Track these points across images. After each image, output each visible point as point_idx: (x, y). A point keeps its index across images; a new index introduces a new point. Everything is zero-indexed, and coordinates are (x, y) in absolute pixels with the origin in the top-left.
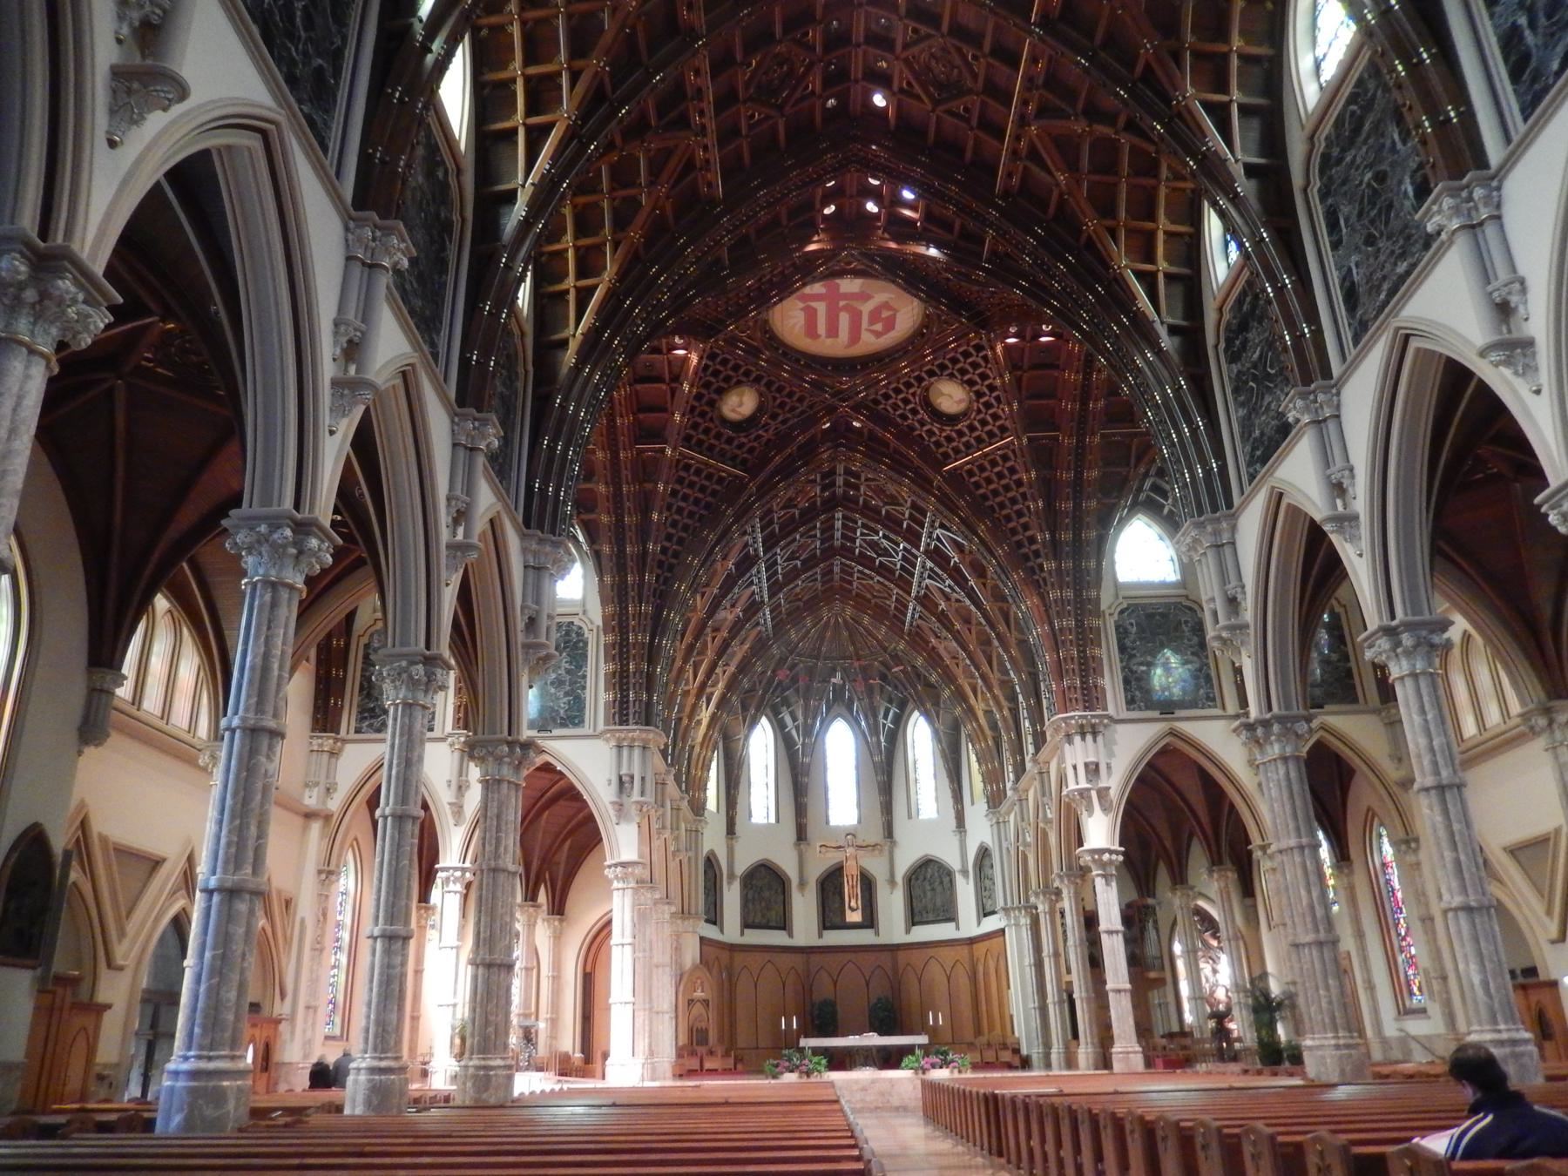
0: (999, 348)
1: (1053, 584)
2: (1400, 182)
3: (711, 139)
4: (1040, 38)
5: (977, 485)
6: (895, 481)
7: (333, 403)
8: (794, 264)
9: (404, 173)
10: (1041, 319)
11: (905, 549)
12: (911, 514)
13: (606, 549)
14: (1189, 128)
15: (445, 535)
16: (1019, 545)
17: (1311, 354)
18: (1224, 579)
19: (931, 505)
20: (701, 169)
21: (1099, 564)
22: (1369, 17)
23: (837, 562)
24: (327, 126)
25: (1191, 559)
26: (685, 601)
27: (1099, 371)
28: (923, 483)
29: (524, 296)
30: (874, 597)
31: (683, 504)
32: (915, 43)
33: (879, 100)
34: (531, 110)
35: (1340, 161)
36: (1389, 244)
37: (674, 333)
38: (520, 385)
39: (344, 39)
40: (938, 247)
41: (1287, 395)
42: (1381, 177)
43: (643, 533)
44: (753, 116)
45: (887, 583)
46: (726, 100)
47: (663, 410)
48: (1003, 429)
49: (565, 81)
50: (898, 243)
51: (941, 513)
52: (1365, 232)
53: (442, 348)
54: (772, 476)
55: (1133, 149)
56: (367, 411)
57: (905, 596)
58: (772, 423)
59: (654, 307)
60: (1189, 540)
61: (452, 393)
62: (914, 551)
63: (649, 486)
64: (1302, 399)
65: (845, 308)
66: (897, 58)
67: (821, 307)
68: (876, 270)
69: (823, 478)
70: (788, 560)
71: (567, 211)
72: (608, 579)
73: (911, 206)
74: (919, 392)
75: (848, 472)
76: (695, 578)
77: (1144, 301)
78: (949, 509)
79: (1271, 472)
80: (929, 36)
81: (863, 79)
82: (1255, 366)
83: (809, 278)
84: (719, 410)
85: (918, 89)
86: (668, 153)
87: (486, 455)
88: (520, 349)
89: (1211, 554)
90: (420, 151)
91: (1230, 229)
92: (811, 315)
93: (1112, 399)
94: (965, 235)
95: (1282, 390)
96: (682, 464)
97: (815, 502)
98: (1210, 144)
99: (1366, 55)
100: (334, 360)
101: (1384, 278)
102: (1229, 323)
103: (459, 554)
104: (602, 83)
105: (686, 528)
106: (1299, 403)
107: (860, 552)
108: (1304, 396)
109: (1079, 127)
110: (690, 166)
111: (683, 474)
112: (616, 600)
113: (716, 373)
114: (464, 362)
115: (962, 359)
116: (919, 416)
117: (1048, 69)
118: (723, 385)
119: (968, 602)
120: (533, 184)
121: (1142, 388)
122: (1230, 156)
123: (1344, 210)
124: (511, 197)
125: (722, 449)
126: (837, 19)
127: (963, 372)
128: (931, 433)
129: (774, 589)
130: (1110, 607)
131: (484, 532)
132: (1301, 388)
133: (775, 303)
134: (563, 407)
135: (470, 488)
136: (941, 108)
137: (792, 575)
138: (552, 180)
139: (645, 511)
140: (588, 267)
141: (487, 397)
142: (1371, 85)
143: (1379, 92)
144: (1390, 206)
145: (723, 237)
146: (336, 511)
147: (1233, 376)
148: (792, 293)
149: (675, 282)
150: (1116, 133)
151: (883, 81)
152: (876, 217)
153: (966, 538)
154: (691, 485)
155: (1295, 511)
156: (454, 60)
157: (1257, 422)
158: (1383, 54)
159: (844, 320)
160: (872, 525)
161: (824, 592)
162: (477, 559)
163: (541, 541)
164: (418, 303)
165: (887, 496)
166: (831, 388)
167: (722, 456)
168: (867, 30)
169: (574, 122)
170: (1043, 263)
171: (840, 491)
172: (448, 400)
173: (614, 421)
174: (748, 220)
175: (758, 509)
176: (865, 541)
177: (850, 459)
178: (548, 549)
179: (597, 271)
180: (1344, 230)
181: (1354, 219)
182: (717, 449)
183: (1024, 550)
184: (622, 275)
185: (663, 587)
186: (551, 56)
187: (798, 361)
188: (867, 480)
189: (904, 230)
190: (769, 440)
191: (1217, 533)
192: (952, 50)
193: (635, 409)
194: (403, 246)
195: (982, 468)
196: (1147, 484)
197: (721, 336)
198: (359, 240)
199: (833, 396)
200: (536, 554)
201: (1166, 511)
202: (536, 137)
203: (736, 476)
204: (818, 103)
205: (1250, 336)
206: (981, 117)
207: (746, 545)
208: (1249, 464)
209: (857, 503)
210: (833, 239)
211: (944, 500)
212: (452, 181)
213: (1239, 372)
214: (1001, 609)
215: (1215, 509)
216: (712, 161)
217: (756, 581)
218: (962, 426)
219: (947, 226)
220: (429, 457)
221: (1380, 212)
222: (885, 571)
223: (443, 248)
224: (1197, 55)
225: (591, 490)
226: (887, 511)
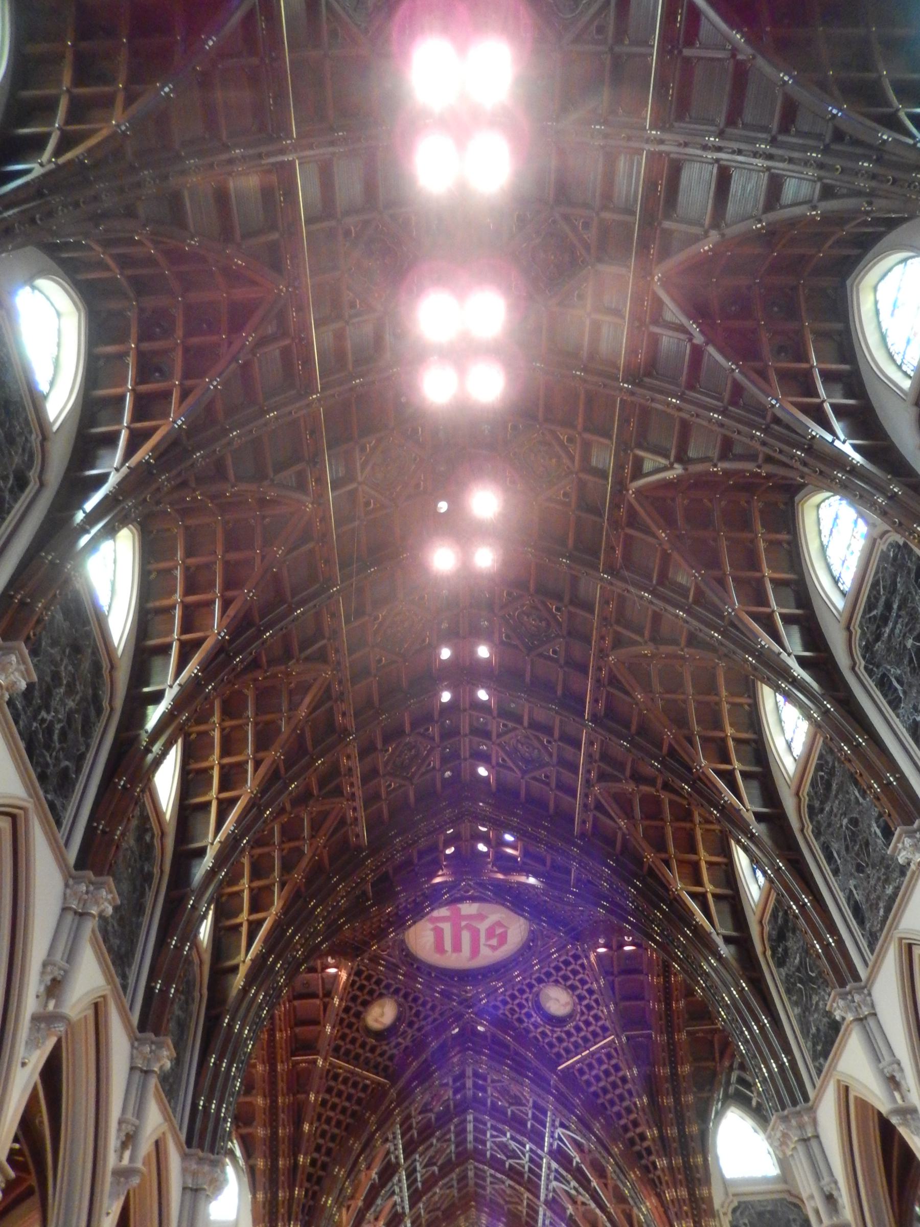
0: (592, 957)
1: (667, 1184)
2: (869, 826)
3: (359, 803)
4: (593, 729)
5: (588, 1083)
6: (517, 1081)
7: (29, 1037)
8: (424, 894)
9: (119, 839)
10: (622, 932)
11: (531, 1150)
12: (533, 1114)
13: (260, 1163)
14: (709, 788)
15: (111, 1161)
16: (632, 1142)
17: (839, 958)
18: (818, 1177)
19: (550, 1103)
20: (351, 825)
21: (705, 1160)
22: (815, 715)
23: (471, 1165)
24: (64, 808)
25: (784, 1154)
26: (332, 1216)
27: (675, 975)
28: (540, 1081)
29: (205, 931)
30: (507, 1202)
31: (331, 1114)
32: (506, 733)
33: (482, 771)
34: (223, 788)
35: (822, 810)
36: (874, 871)
37: (327, 955)
38: (195, 1007)
39: (88, 746)
40: (535, 876)
41: (829, 995)
42: (854, 822)
43: (295, 1147)
44: (390, 785)
45: (517, 1187)
46: (370, 775)
47: (316, 1022)
48: (604, 1029)
49: (250, 767)
50: (505, 874)
51: (560, 1112)
52: (854, 862)
53: (131, 980)
54: (409, 1082)
55: (671, 802)
56: (59, 1041)
57: (535, 1200)
58: (410, 1031)
59: (311, 934)
60: (779, 1135)
61: (135, 1018)
62: (539, 1152)
63: (301, 1097)
64: (843, 999)
65: (468, 927)
66: (493, 743)
67: (447, 927)
68: (489, 896)
69: (455, 1081)
70: (426, 1166)
71: (246, 861)
72: (260, 1196)
73: (513, 846)
74: (531, 996)
75: (476, 1074)
76: (341, 1190)
77: (700, 917)
78: (565, 1106)
79: (833, 1066)
80: (514, 729)
81: (470, 709)
82: (798, 970)
83: (437, 904)
84: (364, 1020)
85: (510, 763)
86: (324, 815)
87: (159, 1077)
88: (198, 979)
89: (801, 1148)
90: (134, 823)
91: (753, 860)
92: (439, 933)
93: (690, 999)
94: (555, 867)
95: (824, 991)
96: (331, 1074)
97: (448, 1106)
98: (726, 799)
99: (820, 741)
100: (38, 997)
101: (879, 898)
102: (770, 935)
103: (122, 1179)
104: (277, 768)
105: (333, 1138)
106: (841, 1003)
107: (492, 1155)
108: (843, 996)
109: (630, 787)
110: (342, 822)
111: (332, 1083)
112: (267, 1219)
113: (362, 988)
114: (149, 990)
115: (564, 967)
116: (533, 1020)
117: (601, 749)
118: (367, 997)
119: (593, 1205)
120: (220, 842)
121: (711, 988)
122: (742, 807)
123: (835, 846)
124: (201, 852)
125: (367, 1058)
126: (449, 719)
127: (566, 978)
128: (544, 1034)
129: (415, 1197)
130: (722, 1206)
131: (149, 1155)
132: (839, 990)
133: (410, 926)
134: (230, 1026)
135: (140, 1112)
136: (527, 777)
137: (430, 1183)
138: (234, 838)
139: (298, 1125)
140: (258, 904)
141: (165, 1020)
142: (829, 758)
143: (836, 764)
144: (867, 844)
145: (367, 875)
146: (16, 1140)
147: (783, 978)
148: (423, 917)
149: (329, 912)
150: (657, 791)
151: (485, 758)
152: (486, 855)
153: (584, 1136)
154: (339, 1094)
155: (863, 1105)
156: (168, 757)
157: (811, 1019)
158: (831, 739)
159: (466, 937)
160: (500, 1126)
161: (460, 1199)
162: (140, 1186)
163: (201, 1160)
164: (116, 942)
165: (510, 1096)
166: (458, 996)
167: (366, 1065)
168: (471, 725)
169: (255, 795)
170: (618, 887)
171: (470, 1093)
172: (131, 1026)
173: (274, 1035)
174: (387, 861)
175: (398, 1114)
176: (494, 1142)
177: (477, 1062)
178: (206, 1168)
179: (266, 907)
180: (839, 862)
181: (843, 852)
182: (362, 1058)
183: (637, 1148)
184: (286, 910)
185: (311, 1203)
186: (241, 750)
187: (429, 974)
188: (493, 1081)
189: (507, 865)
190: (407, 1047)
191: (801, 1127)
192: (532, 737)
193: (292, 1023)
194: (110, 897)
195: (591, 1066)
196: (734, 1078)
197: (366, 955)
198: (75, 894)
199: (460, 1003)
200: (194, 1174)
201: (754, 1103)
202: (225, 807)
203: (379, 1084)
204: (438, 775)
205: (789, 944)
206: (558, 780)
207: (388, 1153)
208: (815, 1058)
209: (485, 1105)
210: (454, 873)
211: (563, 1101)
212: (157, 842)
213: (787, 975)
214: (624, 1211)
215: (795, 1103)
216: (359, 818)
217: (397, 1190)
218: (570, 1027)
219: (541, 860)
220: (107, 1044)
221: (861, 846)
222: (515, 1174)
223: (143, 894)
224: (704, 740)
225: (250, 1104)
226: (512, 1112)
